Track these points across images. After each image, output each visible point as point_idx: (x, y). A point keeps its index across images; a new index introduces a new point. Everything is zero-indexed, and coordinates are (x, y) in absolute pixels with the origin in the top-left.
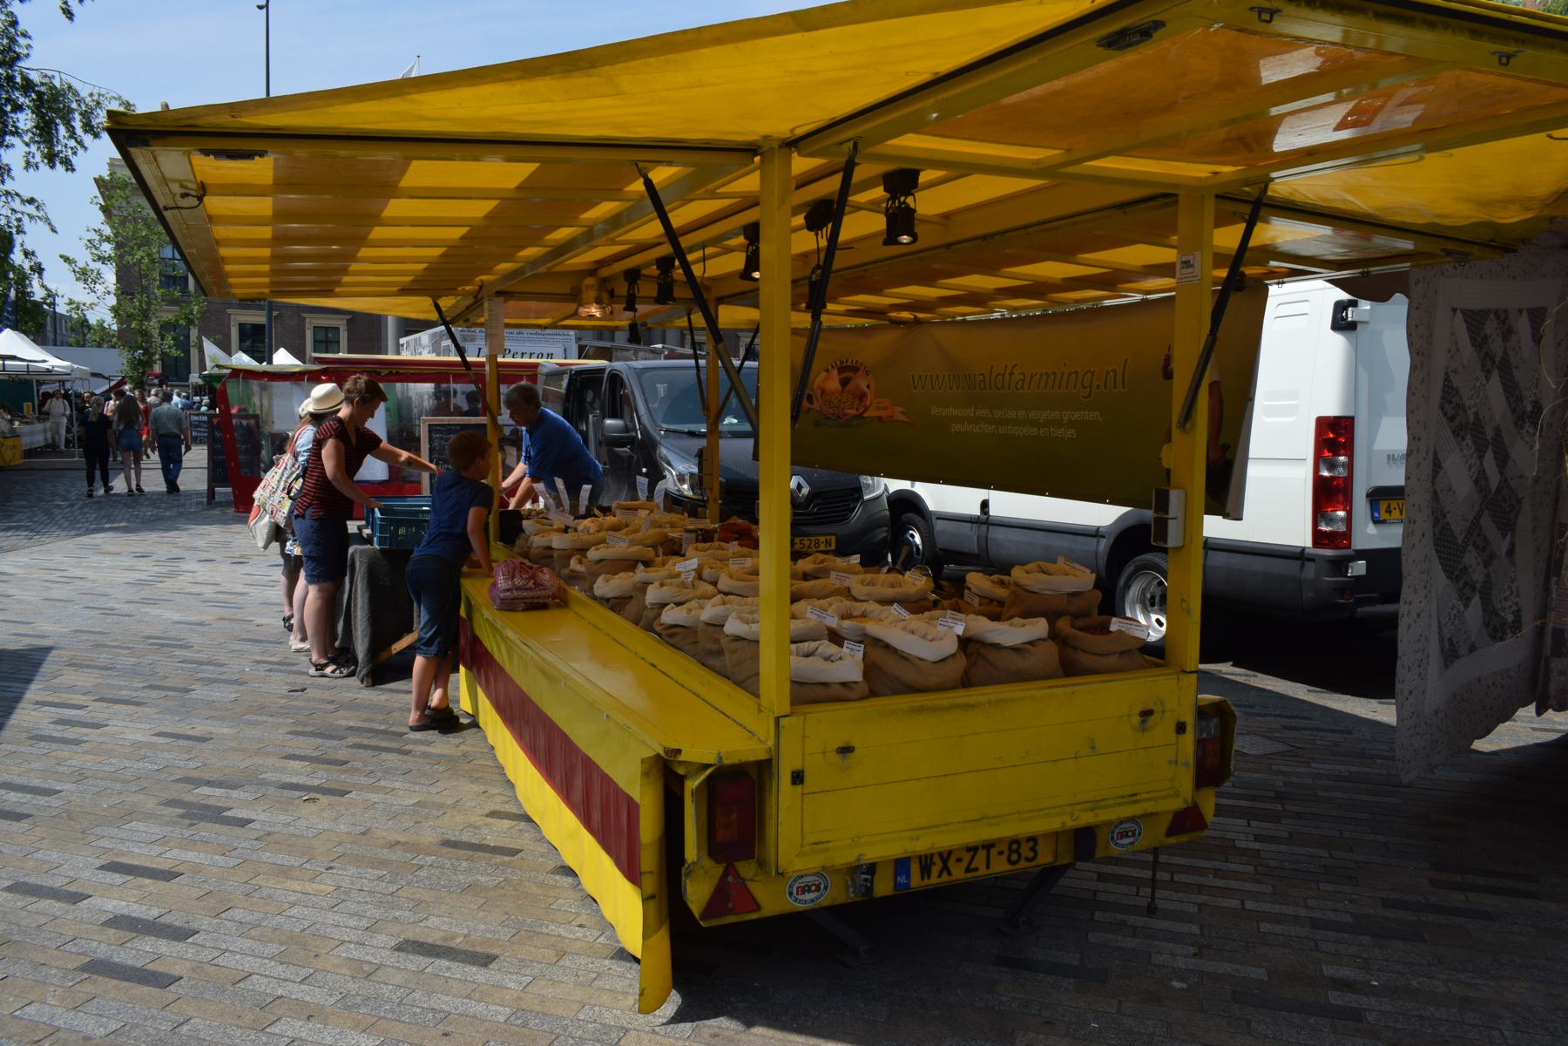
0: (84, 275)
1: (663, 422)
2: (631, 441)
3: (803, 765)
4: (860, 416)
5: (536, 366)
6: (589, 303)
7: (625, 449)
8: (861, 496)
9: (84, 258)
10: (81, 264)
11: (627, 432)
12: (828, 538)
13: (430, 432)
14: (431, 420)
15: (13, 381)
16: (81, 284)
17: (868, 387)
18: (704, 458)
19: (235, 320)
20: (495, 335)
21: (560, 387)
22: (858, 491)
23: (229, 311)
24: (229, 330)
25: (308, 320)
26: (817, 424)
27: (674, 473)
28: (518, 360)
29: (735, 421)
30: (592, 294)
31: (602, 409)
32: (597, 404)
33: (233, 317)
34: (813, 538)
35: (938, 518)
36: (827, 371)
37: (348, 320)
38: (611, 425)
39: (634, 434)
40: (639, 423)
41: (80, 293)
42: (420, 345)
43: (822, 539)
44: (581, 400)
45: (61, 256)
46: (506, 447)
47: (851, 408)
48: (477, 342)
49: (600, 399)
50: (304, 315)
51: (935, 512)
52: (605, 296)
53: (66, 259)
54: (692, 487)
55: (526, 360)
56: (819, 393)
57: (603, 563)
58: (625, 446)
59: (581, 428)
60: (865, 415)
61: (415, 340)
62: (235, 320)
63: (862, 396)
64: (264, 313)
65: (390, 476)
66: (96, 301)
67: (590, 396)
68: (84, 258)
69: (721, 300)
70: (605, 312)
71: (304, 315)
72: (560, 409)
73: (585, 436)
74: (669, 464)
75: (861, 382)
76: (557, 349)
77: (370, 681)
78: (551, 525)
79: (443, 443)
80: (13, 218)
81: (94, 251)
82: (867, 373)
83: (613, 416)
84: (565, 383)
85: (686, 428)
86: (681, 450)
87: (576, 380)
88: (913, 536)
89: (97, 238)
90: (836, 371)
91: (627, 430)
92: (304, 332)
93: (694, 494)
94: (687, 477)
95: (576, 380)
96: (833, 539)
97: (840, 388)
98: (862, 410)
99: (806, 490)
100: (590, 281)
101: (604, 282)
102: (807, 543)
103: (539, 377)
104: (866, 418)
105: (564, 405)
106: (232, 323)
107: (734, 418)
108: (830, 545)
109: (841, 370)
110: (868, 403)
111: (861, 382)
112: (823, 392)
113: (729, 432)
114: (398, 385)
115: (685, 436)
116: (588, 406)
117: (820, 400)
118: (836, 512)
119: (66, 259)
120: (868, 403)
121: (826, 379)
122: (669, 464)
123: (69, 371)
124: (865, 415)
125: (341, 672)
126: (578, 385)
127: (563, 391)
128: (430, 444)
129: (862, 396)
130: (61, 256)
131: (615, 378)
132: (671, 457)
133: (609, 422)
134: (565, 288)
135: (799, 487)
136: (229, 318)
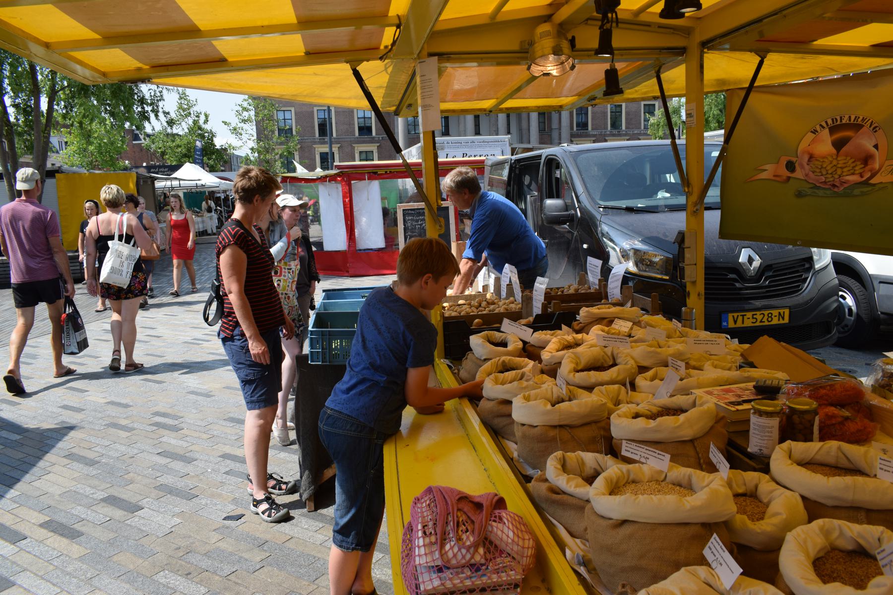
0: (235, 131)
1: (602, 199)
2: (571, 219)
3: (640, 392)
4: (866, 183)
5: (482, 162)
6: (544, 56)
7: (565, 226)
8: (812, 266)
9: (235, 121)
10: (233, 125)
11: (567, 210)
12: (781, 311)
13: (404, 215)
14: (405, 206)
15: (192, 193)
16: (234, 136)
17: (876, 146)
18: (687, 244)
19: (318, 151)
20: (430, 106)
21: (501, 175)
22: (810, 260)
23: (314, 146)
24: (315, 157)
25: (356, 148)
26: (799, 195)
27: (618, 249)
28: (472, 158)
29: (668, 195)
30: (548, 43)
31: (540, 190)
32: (534, 186)
33: (316, 149)
34: (766, 313)
35: (881, 282)
36: (814, 132)
37: (378, 146)
38: (550, 205)
39: (573, 212)
40: (578, 201)
41: (233, 141)
42: (411, 155)
43: (775, 312)
44: (520, 184)
45: (223, 122)
46: (465, 220)
47: (853, 174)
48: (445, 150)
49: (537, 183)
50: (354, 145)
51: (876, 277)
52: (565, 45)
53: (225, 123)
54: (636, 264)
55: (478, 158)
56: (806, 158)
57: (626, 530)
58: (565, 224)
59: (521, 207)
60: (872, 181)
61: (408, 152)
62: (318, 151)
63: (867, 159)
64: (328, 146)
65: (386, 246)
66: (243, 145)
67: (527, 180)
68: (235, 121)
69: (708, 44)
70: (564, 69)
71: (354, 145)
72: (504, 192)
73: (525, 212)
74: (611, 240)
75: (865, 142)
76: (497, 151)
77: (312, 504)
78: (504, 344)
79: (414, 223)
80: (158, 91)
81: (240, 117)
82: (875, 130)
83: (551, 196)
84: (506, 173)
85: (624, 204)
86: (620, 225)
87: (515, 167)
88: (844, 298)
89: (241, 109)
90: (827, 131)
91: (567, 208)
92: (354, 155)
93: (640, 270)
94: (631, 253)
95: (515, 167)
96: (787, 312)
97: (834, 151)
98: (868, 175)
99: (757, 263)
100: (545, 27)
101: (562, 29)
102: (759, 317)
103: (486, 168)
104: (874, 185)
105: (507, 189)
106: (316, 153)
107: (666, 192)
108: (783, 318)
109: (833, 130)
110: (877, 166)
111: (865, 142)
112: (811, 157)
113: (666, 206)
114: (400, 180)
115: (623, 212)
116: (526, 188)
117: (807, 167)
118: (786, 284)
119: (225, 123)
120: (877, 166)
121: (813, 141)
122: (611, 240)
123: (218, 185)
124: (872, 181)
125: (269, 516)
126: (517, 172)
127: (505, 178)
128: (404, 225)
129: (867, 159)
130: (223, 122)
131: (552, 163)
132: (613, 234)
133: (549, 202)
134: (509, 42)
135: (751, 260)
136: (315, 150)
